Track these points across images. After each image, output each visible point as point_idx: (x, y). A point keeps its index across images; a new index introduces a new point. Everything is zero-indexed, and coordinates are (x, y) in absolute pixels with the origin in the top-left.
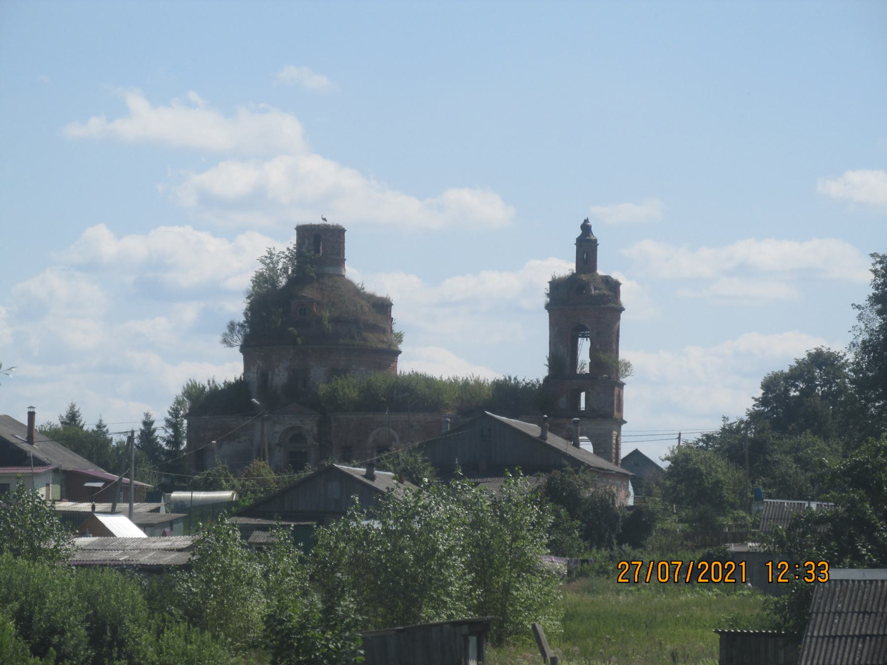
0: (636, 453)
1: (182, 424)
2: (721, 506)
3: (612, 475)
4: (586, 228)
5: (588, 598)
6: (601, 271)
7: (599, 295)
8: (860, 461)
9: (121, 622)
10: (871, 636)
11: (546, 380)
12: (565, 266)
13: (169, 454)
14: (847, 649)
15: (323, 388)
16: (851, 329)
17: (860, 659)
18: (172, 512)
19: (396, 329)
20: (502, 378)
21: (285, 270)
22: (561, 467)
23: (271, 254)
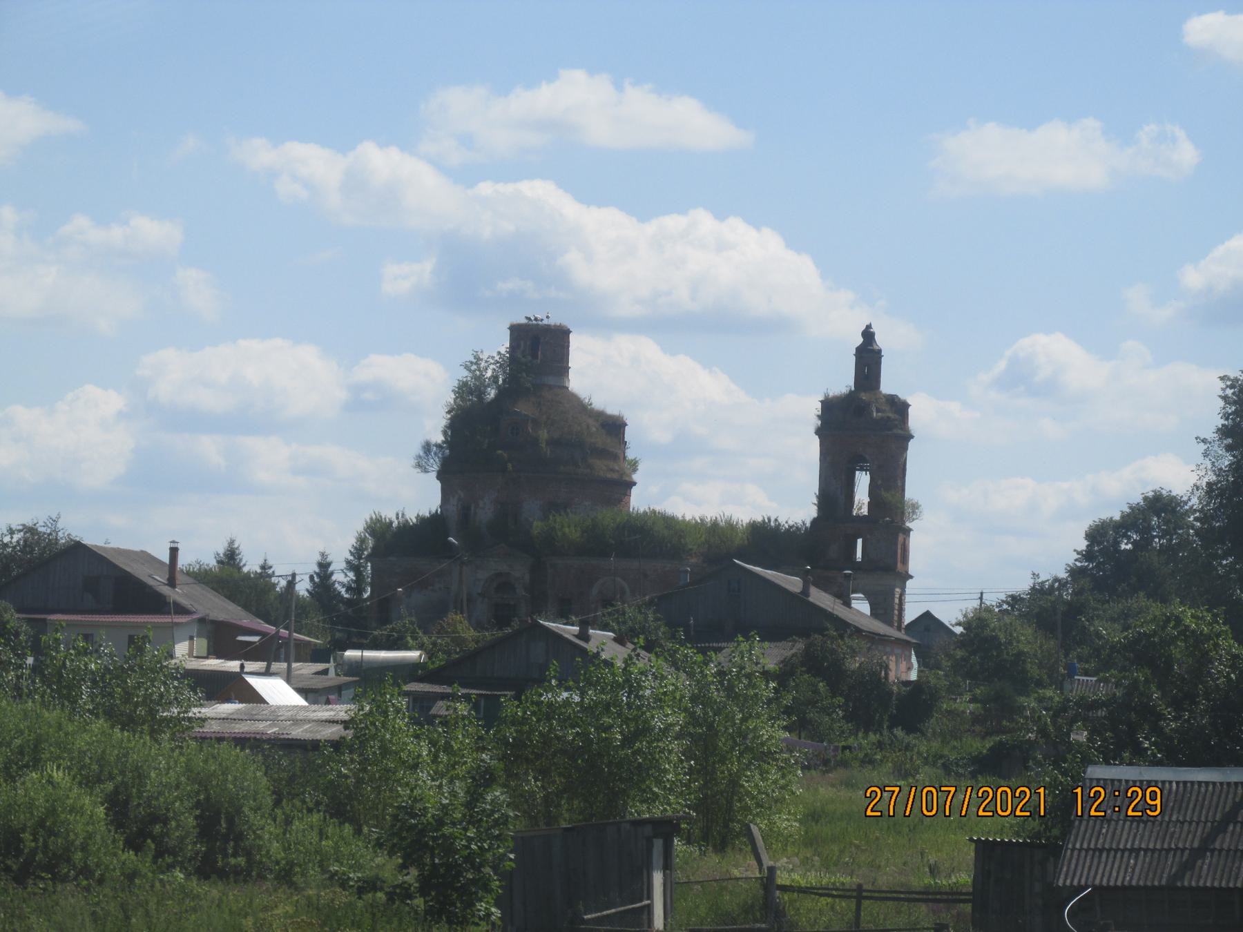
0: (927, 616)
1: (365, 567)
2: (1024, 684)
3: (892, 642)
4: (868, 335)
5: (844, 793)
6: (888, 386)
7: (882, 418)
8: (1145, 633)
9: (239, 811)
10: (1146, 850)
11: (814, 522)
12: (843, 381)
13: (348, 602)
14: (1116, 866)
15: (537, 526)
16: (1194, 468)
17: (1131, 879)
18: (345, 675)
19: (630, 454)
20: (760, 519)
21: (495, 378)
22: (822, 631)
23: (478, 359)
